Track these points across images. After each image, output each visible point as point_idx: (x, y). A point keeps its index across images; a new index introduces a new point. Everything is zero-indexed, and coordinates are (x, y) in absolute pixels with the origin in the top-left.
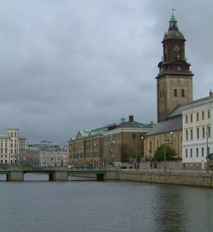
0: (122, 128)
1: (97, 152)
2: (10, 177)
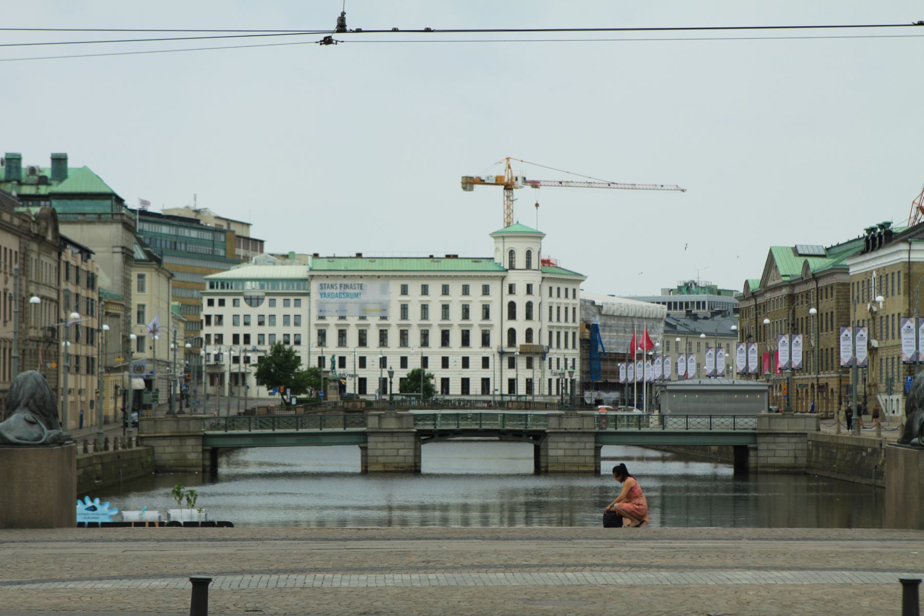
0: (910, 244)
1: (832, 349)
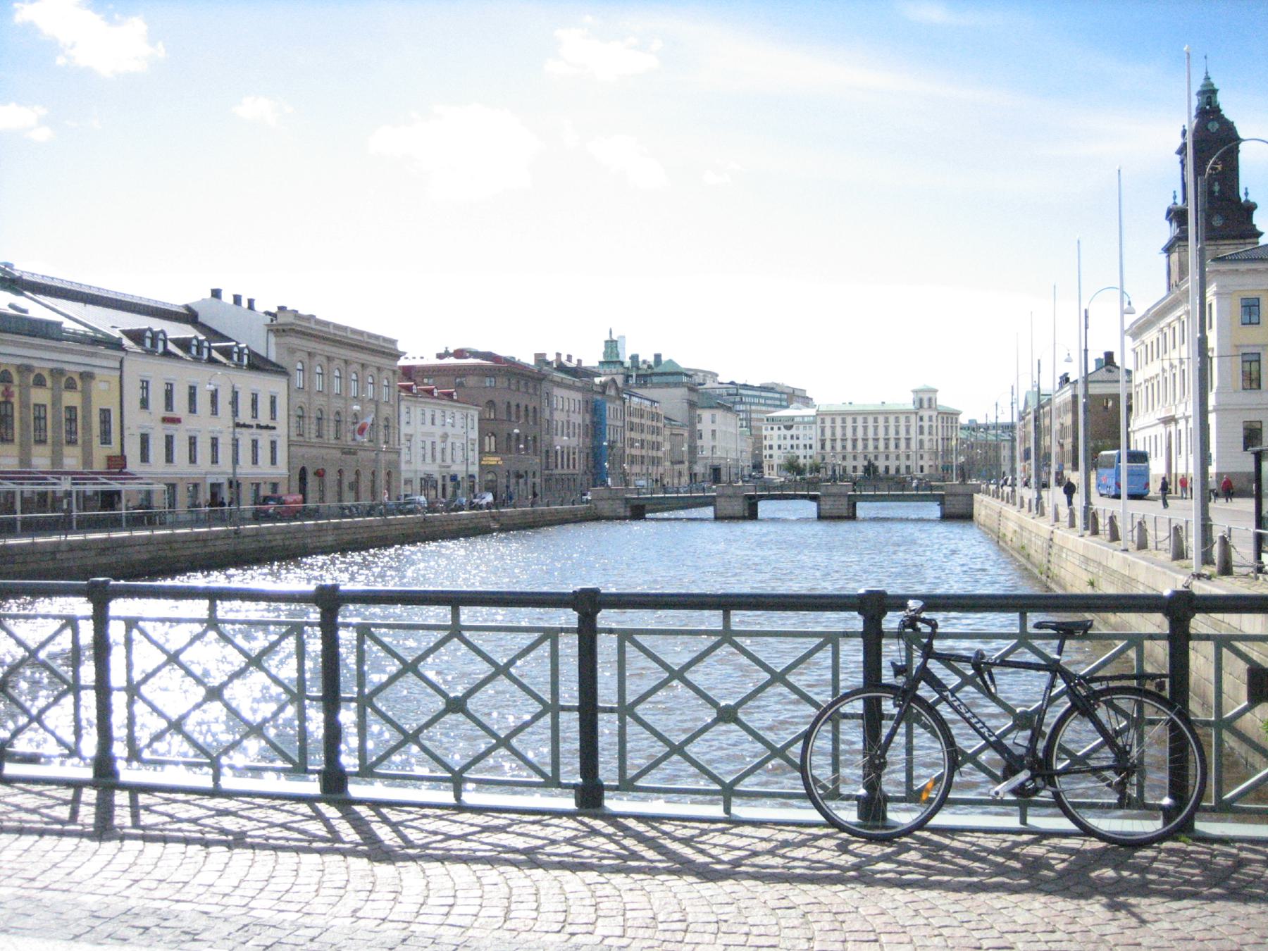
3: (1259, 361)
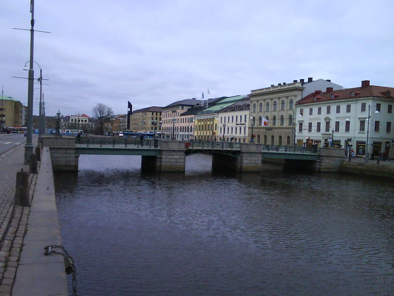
2: (161, 162)
3: (272, 85)
